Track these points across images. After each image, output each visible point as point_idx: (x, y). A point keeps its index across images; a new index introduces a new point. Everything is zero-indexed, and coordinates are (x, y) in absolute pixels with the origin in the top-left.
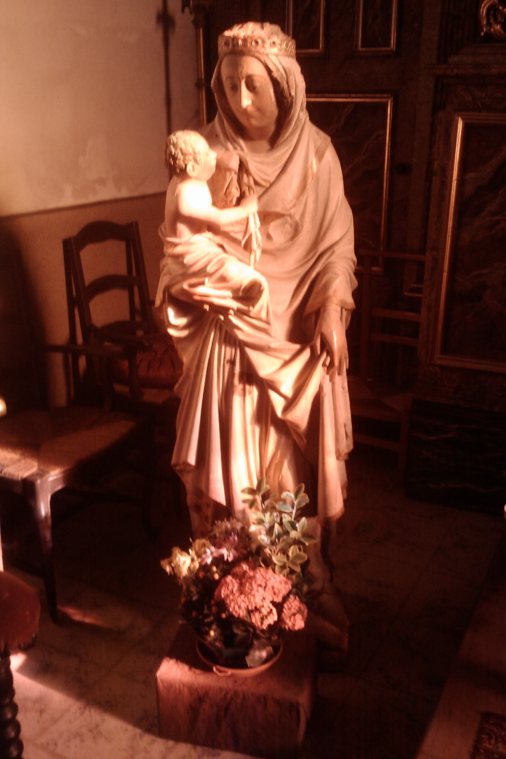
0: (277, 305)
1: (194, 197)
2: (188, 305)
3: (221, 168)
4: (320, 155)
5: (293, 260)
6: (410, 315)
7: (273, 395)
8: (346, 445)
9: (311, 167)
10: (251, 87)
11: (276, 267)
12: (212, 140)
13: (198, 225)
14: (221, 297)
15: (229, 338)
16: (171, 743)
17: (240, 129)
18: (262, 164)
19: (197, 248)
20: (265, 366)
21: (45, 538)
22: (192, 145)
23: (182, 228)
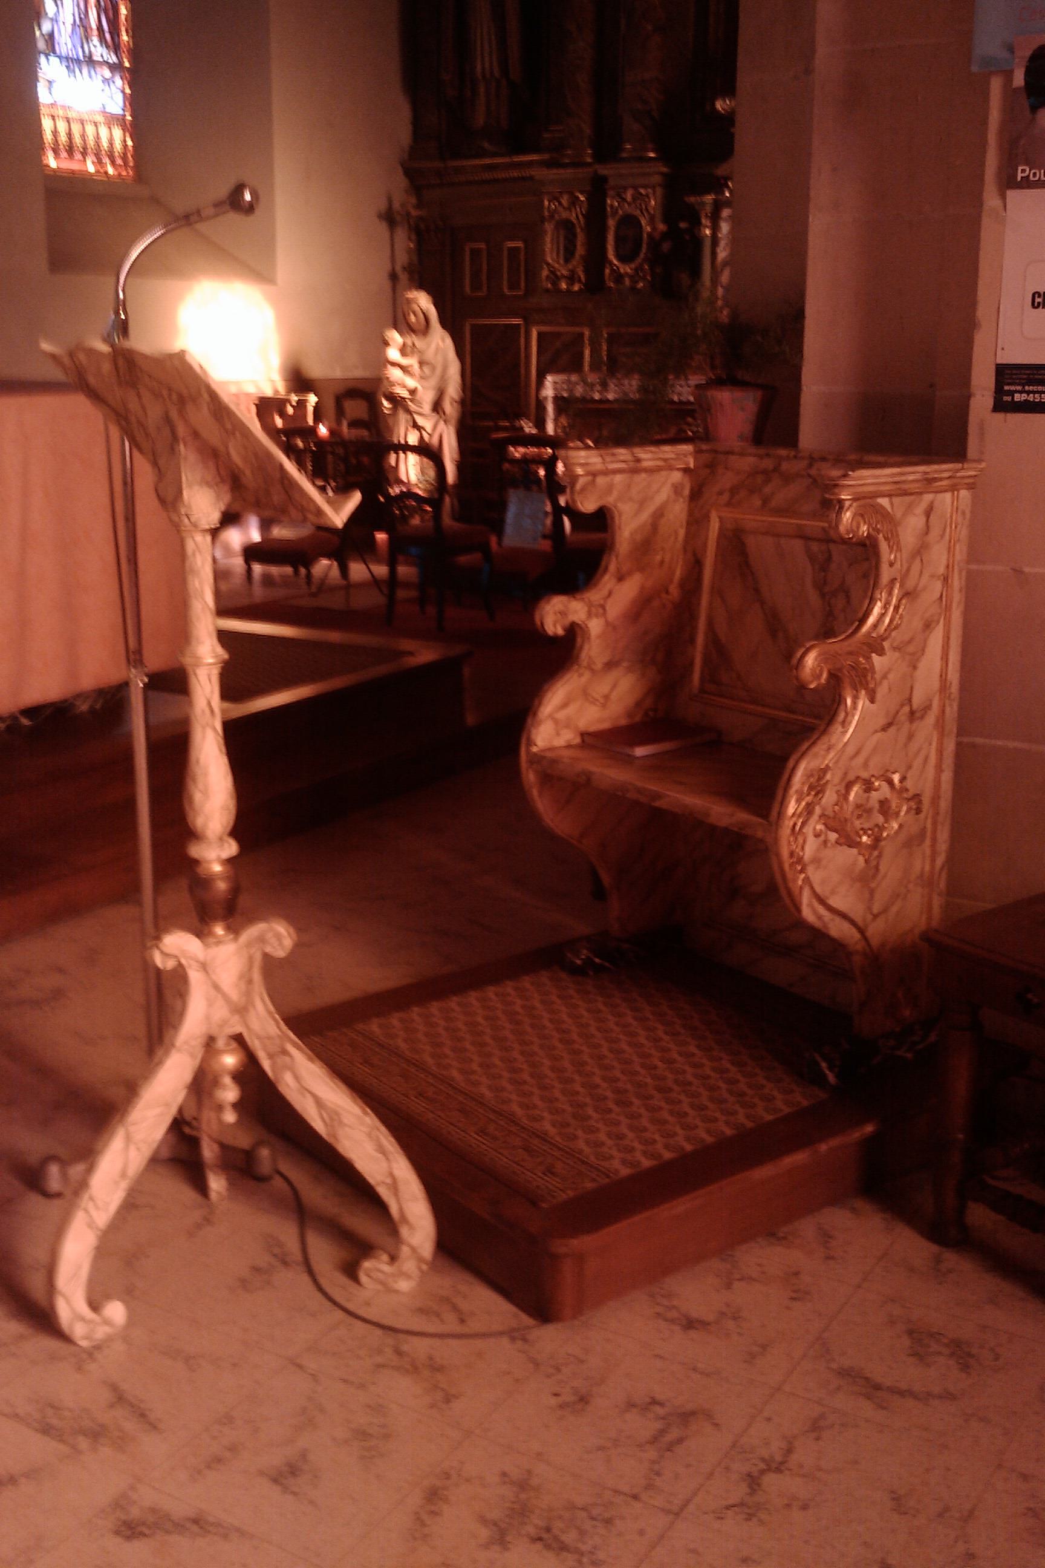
0: (427, 397)
1: (393, 354)
2: (392, 398)
3: (404, 345)
4: (443, 340)
5: (433, 382)
6: (313, 1089)
7: (424, 433)
8: (456, 456)
9: (440, 344)
10: (415, 315)
11: (426, 384)
12: (401, 334)
13: (394, 364)
14: (405, 394)
15: (409, 412)
16: (811, 205)
17: (412, 330)
18: (419, 343)
19: (395, 374)
20: (420, 421)
21: (816, 659)
22: (395, 337)
23: (389, 366)
